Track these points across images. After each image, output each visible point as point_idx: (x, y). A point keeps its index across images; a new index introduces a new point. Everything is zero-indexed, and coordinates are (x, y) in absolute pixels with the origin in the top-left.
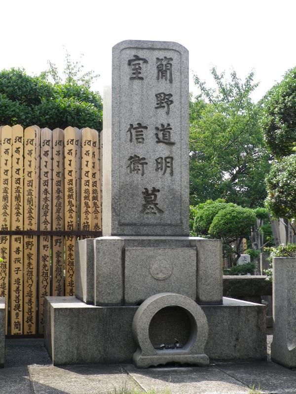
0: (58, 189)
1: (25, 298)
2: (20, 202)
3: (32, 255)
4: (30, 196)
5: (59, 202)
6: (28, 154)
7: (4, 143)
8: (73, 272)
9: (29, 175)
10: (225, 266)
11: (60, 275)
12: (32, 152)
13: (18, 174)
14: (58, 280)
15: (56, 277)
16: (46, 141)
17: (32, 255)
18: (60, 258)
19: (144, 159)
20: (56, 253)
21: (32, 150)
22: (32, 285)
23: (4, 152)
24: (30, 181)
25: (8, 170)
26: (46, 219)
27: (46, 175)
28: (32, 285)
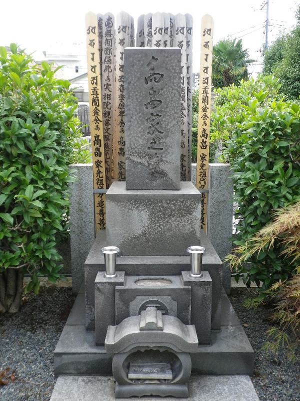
0: (122, 86)
1: (96, 208)
2: (207, 104)
3: (206, 156)
4: (205, 95)
5: (122, 103)
6: (119, 43)
7: (119, 33)
8: (205, 183)
9: (93, 70)
10: (47, 275)
11: (204, 180)
12: (183, 43)
13: (207, 73)
14: (202, 185)
15: (200, 182)
16: (207, 30)
17: (206, 156)
18: (123, 170)
19: (100, 21)
20: (119, 164)
21: (182, 41)
22: (204, 186)
23: (119, 43)
24: (94, 78)
25: (208, 67)
26: (122, 120)
27: (205, 71)
28: (204, 186)
